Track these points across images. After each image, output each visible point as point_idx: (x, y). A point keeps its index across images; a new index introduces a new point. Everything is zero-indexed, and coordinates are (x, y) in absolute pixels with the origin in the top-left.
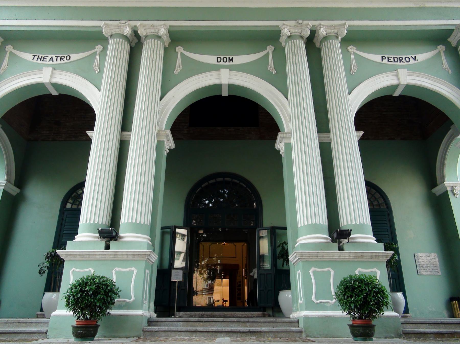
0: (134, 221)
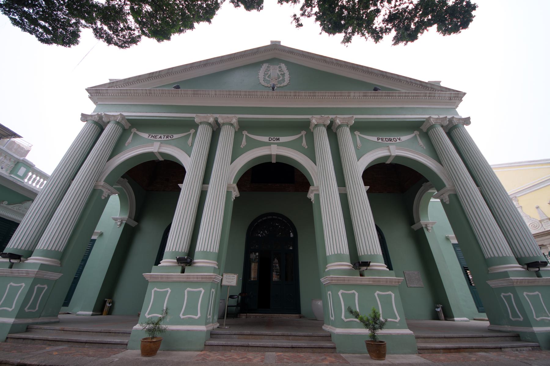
0: (205, 250)
